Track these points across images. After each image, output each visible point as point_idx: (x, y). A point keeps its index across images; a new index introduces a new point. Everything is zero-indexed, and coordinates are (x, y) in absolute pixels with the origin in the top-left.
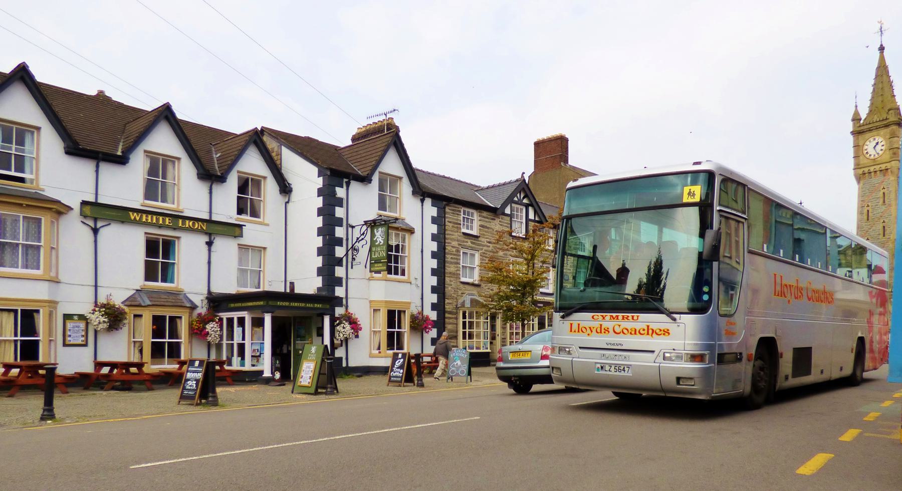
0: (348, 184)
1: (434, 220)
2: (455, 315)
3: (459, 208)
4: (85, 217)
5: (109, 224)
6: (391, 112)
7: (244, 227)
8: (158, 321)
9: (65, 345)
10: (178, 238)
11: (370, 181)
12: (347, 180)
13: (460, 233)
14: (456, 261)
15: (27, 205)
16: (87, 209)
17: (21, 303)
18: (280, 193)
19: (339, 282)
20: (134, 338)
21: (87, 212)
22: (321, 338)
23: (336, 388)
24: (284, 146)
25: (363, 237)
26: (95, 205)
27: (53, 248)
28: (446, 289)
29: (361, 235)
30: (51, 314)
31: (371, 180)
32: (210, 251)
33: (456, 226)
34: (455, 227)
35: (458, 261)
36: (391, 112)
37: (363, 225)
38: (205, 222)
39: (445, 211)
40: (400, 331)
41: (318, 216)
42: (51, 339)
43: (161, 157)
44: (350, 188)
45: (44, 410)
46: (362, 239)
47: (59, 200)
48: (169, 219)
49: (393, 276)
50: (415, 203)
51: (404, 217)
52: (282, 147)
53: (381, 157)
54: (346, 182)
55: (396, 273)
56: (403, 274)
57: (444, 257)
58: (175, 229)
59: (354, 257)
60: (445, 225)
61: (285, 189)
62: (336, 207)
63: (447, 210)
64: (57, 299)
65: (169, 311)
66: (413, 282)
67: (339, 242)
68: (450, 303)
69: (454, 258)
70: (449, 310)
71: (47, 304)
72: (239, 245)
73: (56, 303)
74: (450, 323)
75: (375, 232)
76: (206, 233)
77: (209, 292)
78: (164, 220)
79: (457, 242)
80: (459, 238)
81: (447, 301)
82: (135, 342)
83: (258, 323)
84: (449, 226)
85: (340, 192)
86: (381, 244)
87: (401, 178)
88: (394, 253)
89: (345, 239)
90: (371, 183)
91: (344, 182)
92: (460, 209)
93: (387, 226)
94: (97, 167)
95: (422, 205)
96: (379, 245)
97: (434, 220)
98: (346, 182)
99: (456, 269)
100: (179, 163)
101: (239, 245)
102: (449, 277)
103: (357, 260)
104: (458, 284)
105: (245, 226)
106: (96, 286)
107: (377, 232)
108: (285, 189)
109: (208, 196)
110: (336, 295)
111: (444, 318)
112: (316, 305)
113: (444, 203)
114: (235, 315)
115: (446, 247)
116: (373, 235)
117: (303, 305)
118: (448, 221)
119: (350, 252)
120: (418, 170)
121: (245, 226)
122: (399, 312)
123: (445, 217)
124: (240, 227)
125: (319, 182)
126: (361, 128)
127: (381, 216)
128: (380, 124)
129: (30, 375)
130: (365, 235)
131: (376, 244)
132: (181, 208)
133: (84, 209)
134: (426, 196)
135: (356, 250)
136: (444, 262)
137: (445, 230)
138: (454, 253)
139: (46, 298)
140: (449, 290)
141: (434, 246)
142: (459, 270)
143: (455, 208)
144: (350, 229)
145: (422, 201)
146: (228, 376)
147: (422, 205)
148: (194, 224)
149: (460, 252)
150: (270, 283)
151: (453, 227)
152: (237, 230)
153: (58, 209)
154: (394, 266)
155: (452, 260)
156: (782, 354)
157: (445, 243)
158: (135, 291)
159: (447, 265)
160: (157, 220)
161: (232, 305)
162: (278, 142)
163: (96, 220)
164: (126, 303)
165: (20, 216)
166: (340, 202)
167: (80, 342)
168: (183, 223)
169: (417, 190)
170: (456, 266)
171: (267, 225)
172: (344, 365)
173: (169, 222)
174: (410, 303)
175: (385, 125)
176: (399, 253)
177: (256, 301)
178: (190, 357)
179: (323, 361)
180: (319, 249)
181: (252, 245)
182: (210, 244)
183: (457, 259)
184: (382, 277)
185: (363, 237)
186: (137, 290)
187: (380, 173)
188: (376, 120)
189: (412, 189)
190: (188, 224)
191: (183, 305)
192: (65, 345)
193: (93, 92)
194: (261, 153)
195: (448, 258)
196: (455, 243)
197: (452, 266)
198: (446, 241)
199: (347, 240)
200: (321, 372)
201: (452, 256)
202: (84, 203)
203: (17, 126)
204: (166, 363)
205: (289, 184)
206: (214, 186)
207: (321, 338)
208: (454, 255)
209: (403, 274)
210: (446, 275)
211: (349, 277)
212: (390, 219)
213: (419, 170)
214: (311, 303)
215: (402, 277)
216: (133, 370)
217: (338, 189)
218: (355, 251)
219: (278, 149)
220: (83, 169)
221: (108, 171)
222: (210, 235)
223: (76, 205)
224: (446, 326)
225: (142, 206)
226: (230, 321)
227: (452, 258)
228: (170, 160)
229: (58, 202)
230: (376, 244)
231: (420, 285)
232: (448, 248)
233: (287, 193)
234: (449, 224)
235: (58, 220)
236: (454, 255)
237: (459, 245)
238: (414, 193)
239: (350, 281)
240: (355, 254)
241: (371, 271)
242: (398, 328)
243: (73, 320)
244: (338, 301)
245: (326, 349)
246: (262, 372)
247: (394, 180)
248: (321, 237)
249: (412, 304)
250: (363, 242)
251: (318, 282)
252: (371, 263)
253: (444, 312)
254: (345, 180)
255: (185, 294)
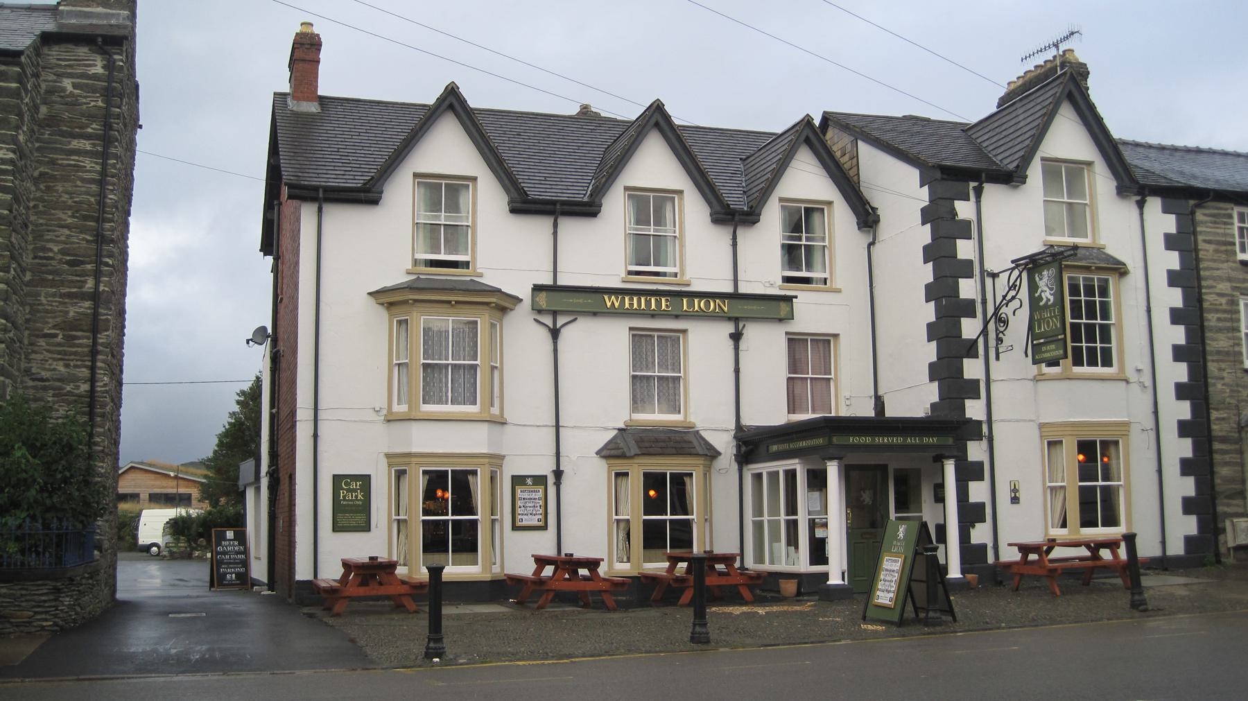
0: (979, 192)
1: (1171, 242)
2: (1236, 443)
3: (1227, 209)
4: (540, 312)
5: (576, 319)
6: (1067, 38)
7: (794, 300)
8: (654, 481)
9: (515, 528)
10: (684, 331)
11: (1023, 180)
12: (976, 184)
13: (1235, 262)
14: (1229, 324)
15: (457, 302)
16: (542, 299)
17: (437, 460)
18: (859, 228)
19: (972, 389)
20: (616, 515)
21: (541, 303)
22: (942, 504)
23: (950, 611)
24: (863, 141)
25: (1012, 293)
26: (554, 289)
27: (493, 368)
28: (1211, 389)
29: (1010, 289)
30: (492, 479)
31: (1026, 177)
32: (737, 349)
33: (1223, 248)
34: (1222, 252)
35: (1235, 324)
36: (1067, 38)
37: (1013, 269)
38: (727, 298)
39: (1193, 220)
40: (1109, 486)
41: (925, 262)
42: (493, 517)
43: (652, 195)
44: (982, 199)
45: (430, 640)
46: (1013, 298)
47: (499, 287)
48: (667, 300)
49: (1086, 370)
50: (1128, 210)
51: (1102, 243)
52: (860, 143)
53: (1043, 129)
54: (974, 188)
55: (1093, 362)
56: (1107, 362)
57: (1202, 319)
58: (677, 317)
59: (1001, 335)
60: (1196, 250)
61: (867, 218)
62: (958, 241)
63: (1200, 215)
64: (503, 453)
65: (671, 465)
66: (1133, 377)
67: (968, 309)
68: (1223, 419)
69: (1225, 320)
70: (1220, 434)
71: (487, 460)
72: (787, 333)
73: (502, 457)
74: (1226, 464)
75: (1037, 279)
76: (730, 319)
77: (739, 427)
78: (658, 303)
79: (1228, 285)
80: (1233, 274)
81: (1214, 415)
82: (618, 521)
83: (818, 481)
84: (1206, 250)
85: (964, 210)
86: (1049, 303)
87: (1089, 164)
88: (1084, 321)
89: (980, 300)
90: (1025, 183)
91: (971, 188)
92: (1229, 211)
93: (1056, 264)
94: (555, 226)
95: (1141, 214)
96: (1046, 306)
97: (1171, 242)
98: (974, 188)
99: (1231, 342)
100: (681, 199)
101: (787, 333)
102: (1217, 361)
103: (1007, 340)
104: (1240, 375)
105: (796, 297)
106: (557, 427)
107: (1041, 279)
108: (867, 218)
109: (730, 249)
110: (968, 415)
111: (1211, 452)
112: (925, 440)
113: (1192, 202)
114: (781, 466)
115: (1205, 297)
116: (1033, 287)
117: (900, 440)
118: (1205, 241)
119: (991, 326)
120: (1125, 143)
121: (796, 297)
122: (1105, 444)
123: (1195, 233)
124: (789, 299)
125: (923, 196)
126: (1015, 82)
127: (1052, 246)
128: (1049, 65)
129: (567, 576)
130: (1017, 288)
131: (1041, 304)
132: (687, 277)
133: (537, 299)
134: (1147, 193)
135: (1004, 322)
136: (1202, 327)
137: (1198, 260)
138: (1224, 307)
139: (484, 450)
140: (1218, 389)
141: (1176, 298)
142: (1239, 345)
143: (1216, 211)
144: (989, 281)
145: (1141, 205)
146: (740, 585)
147: (1141, 214)
148: (708, 305)
149: (1238, 305)
150: (848, 403)
151: (1217, 251)
152: (784, 306)
153: (501, 304)
154: (1082, 343)
155: (1220, 324)
156: (371, 558)
157: (1200, 287)
158: (616, 432)
159: (1208, 334)
160: (648, 303)
161: (774, 448)
162: (851, 135)
163: (555, 314)
164: (603, 454)
165: (449, 320)
166: (964, 230)
167: (536, 523)
168: (691, 305)
169: (1127, 182)
170: (1230, 335)
171: (839, 291)
172: (991, 559)
173: (667, 305)
174: (1127, 424)
175: (1056, 66)
176: (1097, 320)
177: (812, 437)
178: (708, 549)
179: (916, 553)
180: (929, 326)
181: (809, 332)
182: (736, 337)
183: (1231, 320)
184: (1062, 373)
185: (1012, 293)
186: (620, 430)
187: (1043, 159)
188: (1040, 60)
189: (1114, 184)
190: (699, 304)
191: (693, 451)
192: (515, 528)
193: (573, 110)
194: (822, 164)
195: (1209, 320)
196: (1224, 287)
197: (1221, 336)
198: (1204, 283)
199: (984, 302)
200: (913, 578)
201: (1219, 315)
202: (537, 289)
203: (447, 182)
204: (450, 564)
205: (873, 209)
206: (740, 231)
207: (942, 504)
208: (1225, 311)
209: (1107, 362)
210: (1209, 358)
211: (992, 376)
212: (1062, 249)
213: (1137, 145)
214: (915, 437)
215: (1106, 370)
216: (583, 572)
217: (959, 205)
218: (1002, 325)
219: (852, 147)
220: (536, 229)
221: (572, 229)
222: (736, 320)
223: (524, 292)
224: (1217, 469)
225: (623, 282)
226: (774, 476)
227: (1219, 319)
228: (666, 197)
229: (498, 291)
230: (1041, 304)
231: (1149, 383)
232: (1209, 299)
233: (871, 227)
234: (1207, 246)
235: (501, 321)
236: (1225, 311)
237: (1234, 288)
238: (1122, 191)
239: (993, 386)
240: (1002, 329)
241: (1035, 362)
242: (1103, 480)
243: (526, 485)
244: (973, 430)
245: (923, 529)
246: (825, 576)
247: (1076, 169)
248: (933, 303)
249: (1133, 426)
250: (1016, 303)
251: (932, 393)
252: (1033, 346)
253: (1210, 439)
254: (972, 184)
255: (698, 432)
